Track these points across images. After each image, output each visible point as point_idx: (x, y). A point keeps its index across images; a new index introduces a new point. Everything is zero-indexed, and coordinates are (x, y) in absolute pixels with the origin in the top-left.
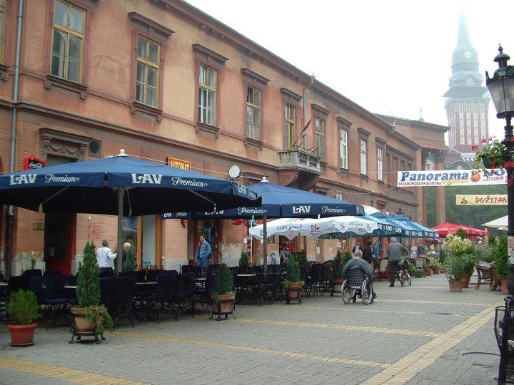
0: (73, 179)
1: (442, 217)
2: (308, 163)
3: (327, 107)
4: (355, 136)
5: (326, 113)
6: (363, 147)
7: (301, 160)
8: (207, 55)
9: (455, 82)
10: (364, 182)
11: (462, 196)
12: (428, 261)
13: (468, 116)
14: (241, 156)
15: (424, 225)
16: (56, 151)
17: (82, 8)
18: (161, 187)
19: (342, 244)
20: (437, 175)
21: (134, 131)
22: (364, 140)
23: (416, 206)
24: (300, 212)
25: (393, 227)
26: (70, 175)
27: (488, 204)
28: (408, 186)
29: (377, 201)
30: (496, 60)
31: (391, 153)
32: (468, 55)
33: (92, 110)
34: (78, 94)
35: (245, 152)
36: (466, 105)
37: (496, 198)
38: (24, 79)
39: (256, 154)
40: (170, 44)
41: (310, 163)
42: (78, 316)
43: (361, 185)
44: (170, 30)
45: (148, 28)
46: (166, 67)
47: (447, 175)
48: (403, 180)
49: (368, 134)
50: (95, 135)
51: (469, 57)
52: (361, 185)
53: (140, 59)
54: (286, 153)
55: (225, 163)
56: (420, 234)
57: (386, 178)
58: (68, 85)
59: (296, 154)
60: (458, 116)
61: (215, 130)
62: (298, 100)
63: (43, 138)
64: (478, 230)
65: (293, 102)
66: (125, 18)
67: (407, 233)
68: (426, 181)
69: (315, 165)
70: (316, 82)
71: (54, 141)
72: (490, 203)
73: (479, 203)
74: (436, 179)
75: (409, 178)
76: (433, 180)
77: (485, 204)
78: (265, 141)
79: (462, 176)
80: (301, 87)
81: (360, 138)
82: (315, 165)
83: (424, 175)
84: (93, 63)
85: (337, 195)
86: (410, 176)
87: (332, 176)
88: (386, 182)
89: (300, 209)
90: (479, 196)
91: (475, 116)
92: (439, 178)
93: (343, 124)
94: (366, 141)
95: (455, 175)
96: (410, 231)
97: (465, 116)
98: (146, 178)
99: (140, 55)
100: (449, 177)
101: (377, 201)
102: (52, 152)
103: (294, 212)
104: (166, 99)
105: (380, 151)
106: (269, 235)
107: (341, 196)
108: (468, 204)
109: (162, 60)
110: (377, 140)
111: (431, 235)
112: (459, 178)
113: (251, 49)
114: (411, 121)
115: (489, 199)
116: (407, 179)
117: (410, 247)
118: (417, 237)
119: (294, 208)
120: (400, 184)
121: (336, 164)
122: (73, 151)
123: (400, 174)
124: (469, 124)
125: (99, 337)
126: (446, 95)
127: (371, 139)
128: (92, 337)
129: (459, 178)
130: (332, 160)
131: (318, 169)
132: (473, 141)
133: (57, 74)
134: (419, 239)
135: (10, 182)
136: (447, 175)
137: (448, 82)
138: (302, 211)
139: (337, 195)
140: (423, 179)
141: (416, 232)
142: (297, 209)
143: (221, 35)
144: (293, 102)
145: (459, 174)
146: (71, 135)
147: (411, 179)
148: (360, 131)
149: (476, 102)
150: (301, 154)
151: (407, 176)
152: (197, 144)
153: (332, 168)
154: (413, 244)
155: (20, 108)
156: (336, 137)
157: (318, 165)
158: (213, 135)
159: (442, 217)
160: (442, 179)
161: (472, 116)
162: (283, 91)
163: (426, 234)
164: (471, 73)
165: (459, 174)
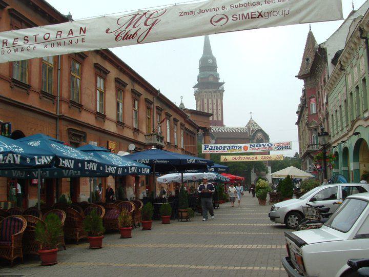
0: (166, 162)
2: (310, 166)
5: (162, 110)
9: (202, 78)
13: (210, 101)
20: (224, 147)
22: (101, 77)
25: (99, 165)
26: (165, 160)
31: (186, 131)
32: (210, 61)
36: (209, 94)
38: (62, 102)
44: (107, 70)
48: (205, 149)
50: (84, 130)
54: (149, 135)
55: (127, 142)
59: (155, 136)
60: (203, 101)
61: (53, 97)
62: (151, 104)
63: (69, 134)
66: (93, 66)
71: (74, 135)
73: (235, 160)
74: (224, 149)
75: (208, 148)
77: (238, 160)
80: (152, 97)
83: (217, 147)
84: (83, 92)
91: (215, 102)
94: (105, 79)
98: (191, 161)
103: (37, 163)
104: (107, 110)
105: (182, 131)
106: (184, 181)
112: (237, 149)
116: (208, 149)
119: (86, 163)
123: (203, 146)
125: (188, 220)
128: (187, 219)
129: (237, 149)
132: (218, 118)
145: (237, 147)
149: (215, 92)
150: (158, 137)
155: (62, 118)
162: (146, 100)
164: (212, 73)
165: (237, 147)
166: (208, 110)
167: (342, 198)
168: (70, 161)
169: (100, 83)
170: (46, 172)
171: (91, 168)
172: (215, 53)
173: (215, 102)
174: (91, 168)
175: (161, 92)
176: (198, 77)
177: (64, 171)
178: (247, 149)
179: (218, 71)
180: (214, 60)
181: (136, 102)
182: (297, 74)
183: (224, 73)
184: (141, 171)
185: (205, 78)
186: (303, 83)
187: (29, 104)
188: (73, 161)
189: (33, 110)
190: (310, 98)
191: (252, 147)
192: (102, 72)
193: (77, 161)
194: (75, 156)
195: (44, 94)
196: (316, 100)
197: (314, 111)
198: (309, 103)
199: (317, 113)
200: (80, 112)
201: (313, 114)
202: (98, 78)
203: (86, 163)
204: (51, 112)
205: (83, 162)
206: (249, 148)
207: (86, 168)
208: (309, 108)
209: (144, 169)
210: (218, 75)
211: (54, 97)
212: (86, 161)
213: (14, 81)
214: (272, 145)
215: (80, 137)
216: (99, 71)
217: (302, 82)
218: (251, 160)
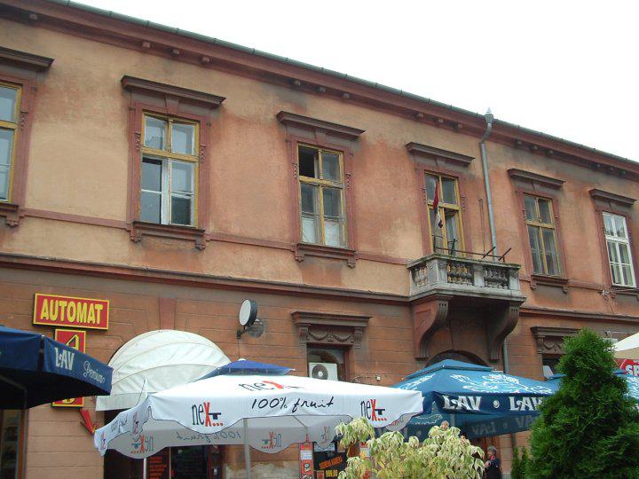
3: (557, 174)
5: (556, 185)
8: (434, 157)
14: (291, 281)
16: (320, 340)
17: (13, 83)
18: (70, 375)
21: (174, 274)
24: (523, 409)
33: (584, 303)
34: (560, 289)
35: (299, 274)
39: (337, 276)
40: (51, 82)
45: (435, 160)
46: (36, 125)
53: (529, 222)
58: (324, 252)
61: (560, 283)
63: (298, 326)
70: (498, 125)
78: (363, 247)
82: (506, 284)
89: (524, 402)
93: (603, 201)
99: (529, 217)
102: (312, 340)
109: (557, 219)
113: (597, 161)
119: (512, 399)
121: (598, 278)
122: (342, 338)
133: (188, 223)
135: (482, 400)
138: (527, 408)
142: (518, 403)
143: (532, 145)
146: (321, 316)
152: (134, 265)
156: (592, 230)
158: (190, 246)
166: (544, 273)
167: (90, 398)
168: (69, 353)
171: (64, 365)
174: (64, 365)
177: (517, 419)
187: (366, 290)
188: (73, 354)
193: (487, 398)
195: (540, 281)
203: (512, 399)
204: (549, 308)
209: (60, 352)
211: (565, 282)
213: (302, 247)
215: (351, 330)
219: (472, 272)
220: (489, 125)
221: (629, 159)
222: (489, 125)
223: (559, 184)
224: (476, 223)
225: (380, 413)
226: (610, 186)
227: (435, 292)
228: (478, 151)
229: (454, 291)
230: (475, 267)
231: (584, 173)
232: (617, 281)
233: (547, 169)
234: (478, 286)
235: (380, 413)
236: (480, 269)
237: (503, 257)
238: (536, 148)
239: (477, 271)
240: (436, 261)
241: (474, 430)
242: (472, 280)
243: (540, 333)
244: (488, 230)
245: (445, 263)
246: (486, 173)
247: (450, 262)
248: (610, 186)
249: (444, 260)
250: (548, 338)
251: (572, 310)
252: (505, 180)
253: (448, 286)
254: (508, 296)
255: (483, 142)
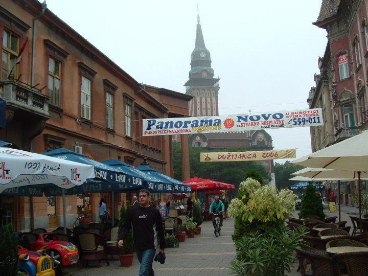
1: (187, 172)
4: (100, 88)
5: (64, 55)
6: (109, 99)
7: (17, 96)
9: (194, 74)
10: (110, 136)
11: (206, 154)
12: (180, 221)
13: (203, 100)
15: (171, 176)
19: (85, 201)
20: (186, 123)
22: (110, 93)
23: (164, 164)
25: (128, 176)
27: (229, 160)
28: (155, 135)
29: (125, 157)
30: (217, 80)
31: (140, 113)
32: (203, 55)
37: (236, 155)
41: (34, 103)
42: (32, 225)
43: (107, 138)
47: (197, 122)
48: (149, 128)
49: (114, 88)
51: (204, 56)
52: (107, 138)
56: (169, 188)
57: (134, 135)
59: (10, 87)
64: (225, 184)
65: (18, 31)
67: (151, 186)
68: (174, 129)
69: (42, 107)
70: (48, 13)
72: (231, 159)
73: (222, 160)
75: (154, 126)
76: (182, 128)
77: (226, 160)
79: (213, 122)
80: (31, 17)
81: (106, 91)
82: (42, 107)
83: (172, 123)
85: (76, 147)
86: (156, 124)
87: (70, 126)
88: (134, 139)
90: (222, 154)
92: (189, 125)
94: (113, 95)
95: (206, 122)
96: (156, 183)
97: (201, 100)
100: (199, 124)
101: (125, 157)
107: (80, 148)
108: (211, 161)
109: (62, 74)
110: (125, 96)
111: (183, 189)
114: (159, 89)
115: (230, 156)
116: (153, 128)
117: (159, 201)
118: (165, 191)
120: (145, 133)
124: (204, 106)
126: (186, 85)
127: (119, 93)
129: (210, 125)
130: (71, 106)
131: (45, 111)
134: (168, 194)
136: (197, 122)
137: (188, 75)
139: (76, 147)
140: (171, 127)
141: (164, 184)
144: (18, 31)
145: (211, 121)
147: (157, 127)
148: (106, 82)
149: (208, 90)
150: (19, 89)
151: (153, 124)
153: (71, 117)
154: (162, 198)
156: (76, 84)
157: (46, 108)
159: (187, 172)
160: (192, 126)
161: (206, 100)
163: (177, 187)
164: (205, 68)
165: (211, 121)
169: (109, 99)
170: (98, 186)
171: (121, 180)
172: (208, 46)
173: (209, 100)
174: (121, 180)
175: (49, 7)
176: (190, 74)
178: (232, 125)
179: (213, 66)
180: (208, 54)
181: (60, 65)
182: (315, 20)
183: (218, 68)
184: (132, 181)
185: (197, 74)
186: (326, 34)
188: (106, 173)
189: (57, 130)
190: (338, 56)
191: (242, 121)
192: (87, 73)
194: (179, 183)
196: (349, 58)
197: (344, 75)
198: (337, 62)
199: (351, 78)
200: (114, 136)
201: (344, 80)
202: (126, 105)
205: (114, 173)
206: (236, 124)
207: (117, 180)
208: (336, 71)
209: (135, 179)
210: (213, 70)
211: (61, 111)
212: (117, 172)
214: (281, 116)
216: (126, 100)
217: (323, 32)
218: (247, 160)
219: (27, 96)
220: (44, 10)
221: (88, 40)
222: (44, 10)
223: (27, 28)
224: (25, 67)
225: (7, 173)
226: (87, 62)
227: (9, 104)
228: (32, 22)
229: (19, 106)
230: (30, 94)
231: (77, 52)
232: (85, 116)
233: (62, 45)
234: (29, 105)
235: (7, 173)
236: (32, 95)
237: (41, 91)
238: (60, 31)
239: (30, 96)
240: (11, 85)
241: (51, 191)
242: (26, 101)
243: (48, 138)
244: (30, 72)
245: (16, 87)
246: (35, 38)
247: (18, 87)
248: (87, 62)
249: (15, 85)
250: (52, 142)
251: (63, 127)
252: (42, 45)
253: (15, 102)
254: (43, 114)
255: (36, 19)
